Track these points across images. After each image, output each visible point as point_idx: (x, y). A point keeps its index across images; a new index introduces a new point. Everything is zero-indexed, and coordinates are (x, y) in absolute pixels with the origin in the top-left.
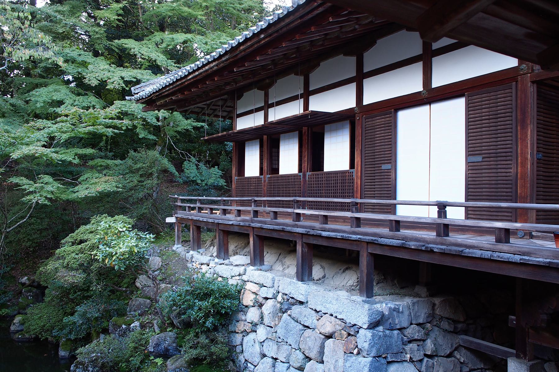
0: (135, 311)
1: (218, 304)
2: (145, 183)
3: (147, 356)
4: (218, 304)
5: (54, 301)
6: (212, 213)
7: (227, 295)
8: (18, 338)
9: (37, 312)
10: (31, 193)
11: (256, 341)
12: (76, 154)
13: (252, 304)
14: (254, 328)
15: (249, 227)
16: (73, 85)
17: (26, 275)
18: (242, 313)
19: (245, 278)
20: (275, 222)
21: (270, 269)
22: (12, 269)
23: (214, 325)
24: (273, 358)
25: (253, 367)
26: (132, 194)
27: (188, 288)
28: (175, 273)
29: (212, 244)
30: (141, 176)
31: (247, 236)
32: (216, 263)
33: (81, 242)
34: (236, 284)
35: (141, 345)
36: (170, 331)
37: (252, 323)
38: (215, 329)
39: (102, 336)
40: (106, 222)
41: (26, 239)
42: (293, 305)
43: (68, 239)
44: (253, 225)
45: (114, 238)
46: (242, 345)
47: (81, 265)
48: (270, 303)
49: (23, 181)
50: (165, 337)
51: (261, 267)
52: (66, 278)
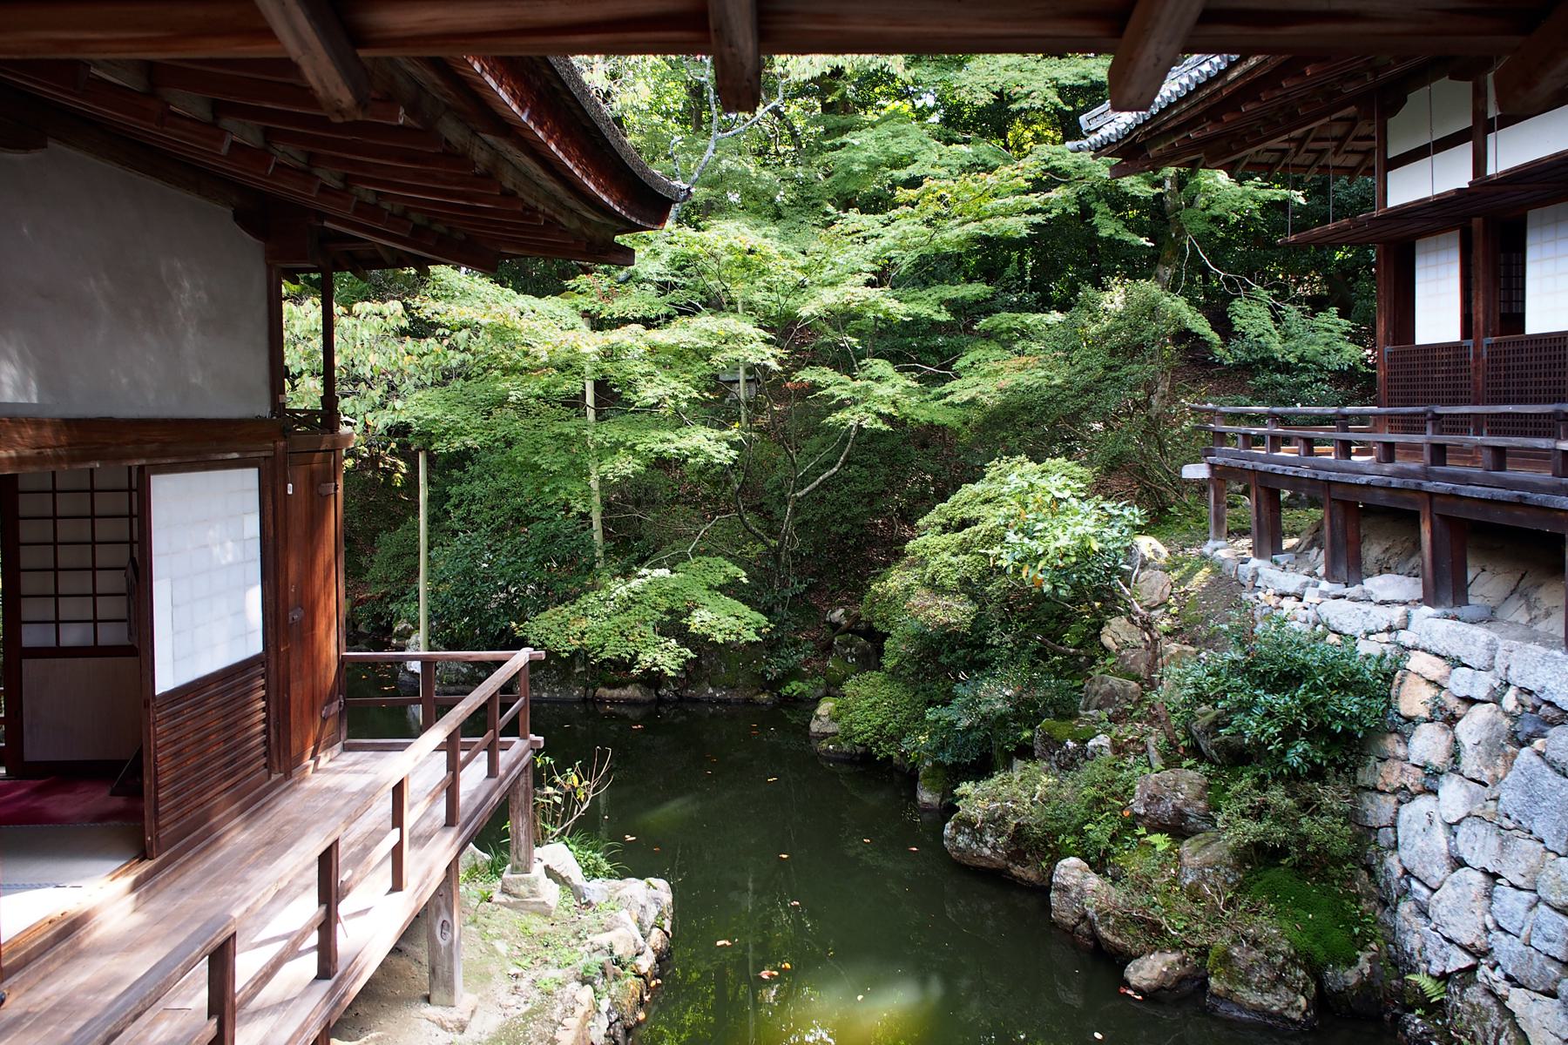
0: (1099, 708)
1: (1324, 704)
2: (1125, 370)
3: (1131, 824)
4: (1324, 704)
5: (904, 668)
6: (1310, 452)
7: (1350, 683)
8: (827, 751)
9: (866, 692)
10: (841, 405)
11: (1437, 819)
12: (942, 302)
13: (1426, 715)
14: (1430, 783)
15: (1418, 491)
16: (935, 118)
17: (841, 605)
18: (1395, 737)
19: (1406, 638)
20: (1498, 478)
21: (1489, 618)
22: (810, 588)
23: (1312, 762)
24: (1485, 872)
25: (1425, 891)
26: (1092, 403)
27: (1237, 656)
28: (1208, 617)
29: (1314, 540)
30: (1113, 352)
31: (1412, 519)
32: (1323, 594)
33: (964, 524)
34: (1378, 653)
35: (1114, 794)
36: (1190, 768)
37: (1423, 768)
38: (1317, 773)
39: (1018, 764)
40: (1022, 476)
41: (838, 516)
42: (1552, 724)
43: (932, 517)
44: (1429, 486)
45: (1040, 510)
46: (1394, 826)
47: (965, 582)
48: (1481, 713)
49: (824, 376)
50: (1176, 780)
51: (1457, 611)
52: (931, 612)
